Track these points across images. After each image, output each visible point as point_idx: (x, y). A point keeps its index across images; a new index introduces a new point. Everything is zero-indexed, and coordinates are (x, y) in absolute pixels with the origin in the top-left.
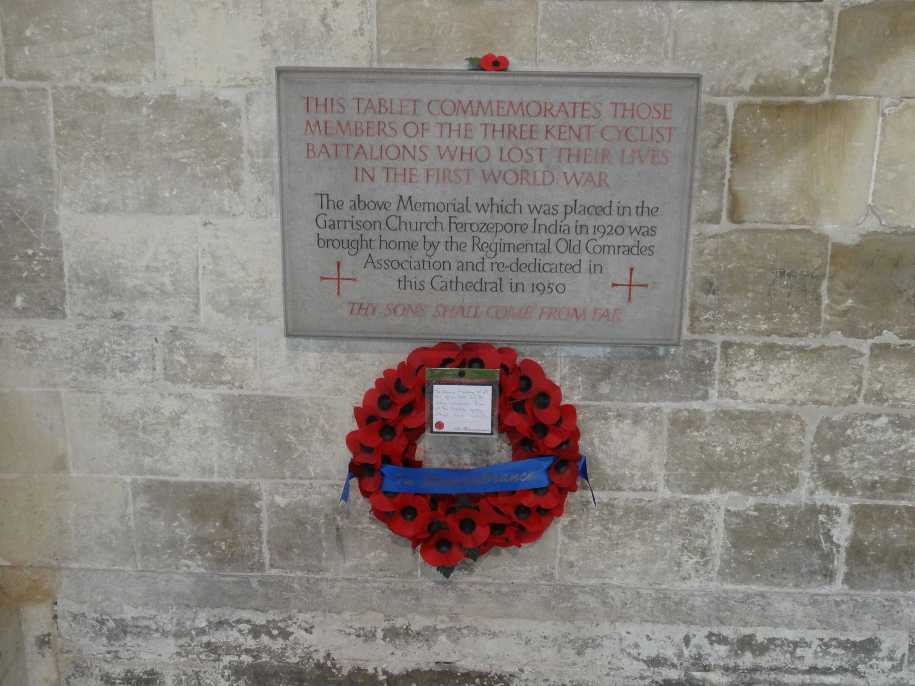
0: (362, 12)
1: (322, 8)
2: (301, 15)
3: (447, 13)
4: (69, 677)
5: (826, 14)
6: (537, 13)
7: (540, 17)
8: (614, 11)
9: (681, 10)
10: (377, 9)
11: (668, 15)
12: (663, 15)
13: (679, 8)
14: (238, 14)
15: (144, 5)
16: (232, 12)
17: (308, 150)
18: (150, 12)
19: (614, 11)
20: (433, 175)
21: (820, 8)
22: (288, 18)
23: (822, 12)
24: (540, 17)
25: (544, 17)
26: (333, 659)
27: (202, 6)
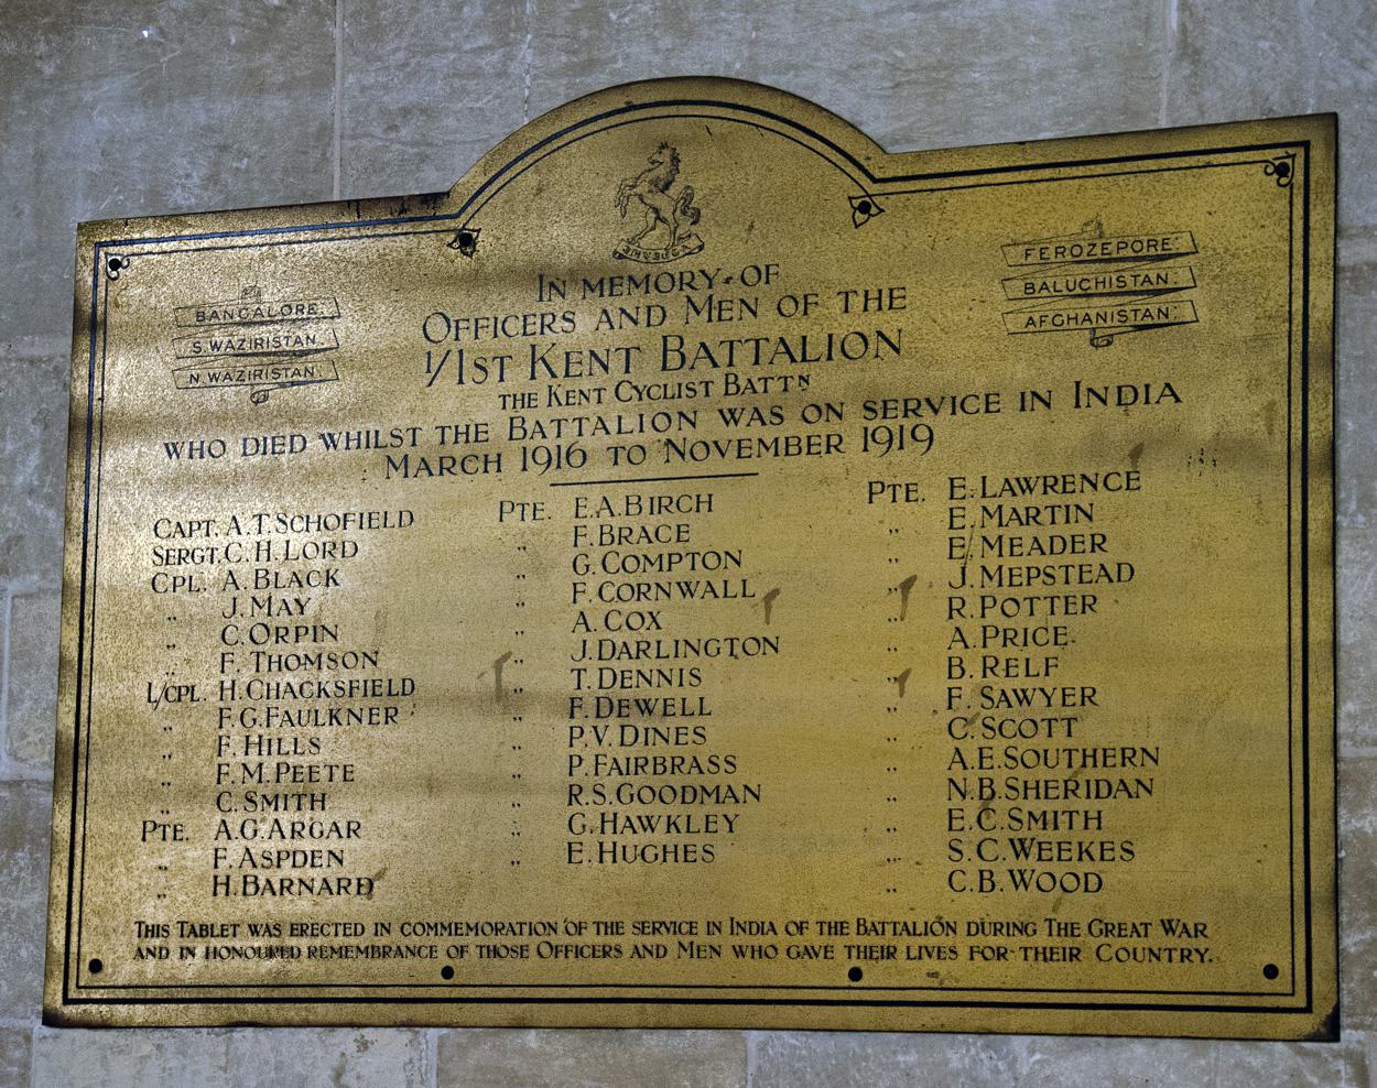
0: (411, 1061)
1: (337, 1054)
2: (299, 1068)
3: (571, 1061)
4: (682, 344)
5: (1350, 1070)
6: (745, 1062)
7: (751, 1069)
8: (900, 1058)
9: (1037, 1057)
10: (440, 1053)
11: (1012, 1065)
12: (1002, 1066)
13: (1032, 1052)
14: (184, 1068)
15: (18, 1054)
16: (173, 1063)
17: (727, 383)
18: (26, 1066)
19: (900, 1058)
20: (643, 1012)
21: (1337, 1056)
22: (273, 1075)
23: (1341, 1065)
24: (751, 1069)
25: (759, 1068)
26: (571, 272)
27: (121, 1052)
